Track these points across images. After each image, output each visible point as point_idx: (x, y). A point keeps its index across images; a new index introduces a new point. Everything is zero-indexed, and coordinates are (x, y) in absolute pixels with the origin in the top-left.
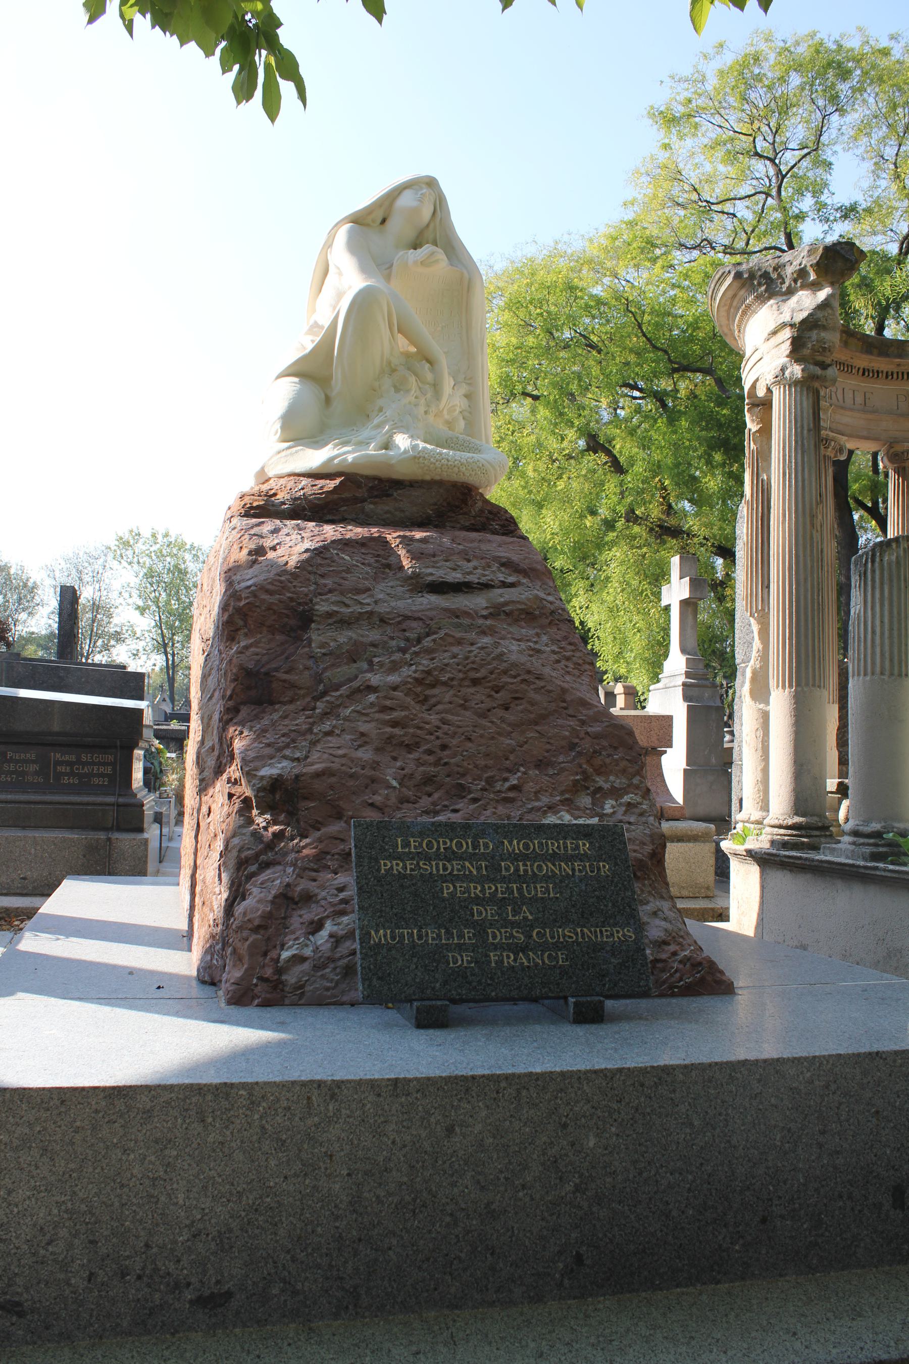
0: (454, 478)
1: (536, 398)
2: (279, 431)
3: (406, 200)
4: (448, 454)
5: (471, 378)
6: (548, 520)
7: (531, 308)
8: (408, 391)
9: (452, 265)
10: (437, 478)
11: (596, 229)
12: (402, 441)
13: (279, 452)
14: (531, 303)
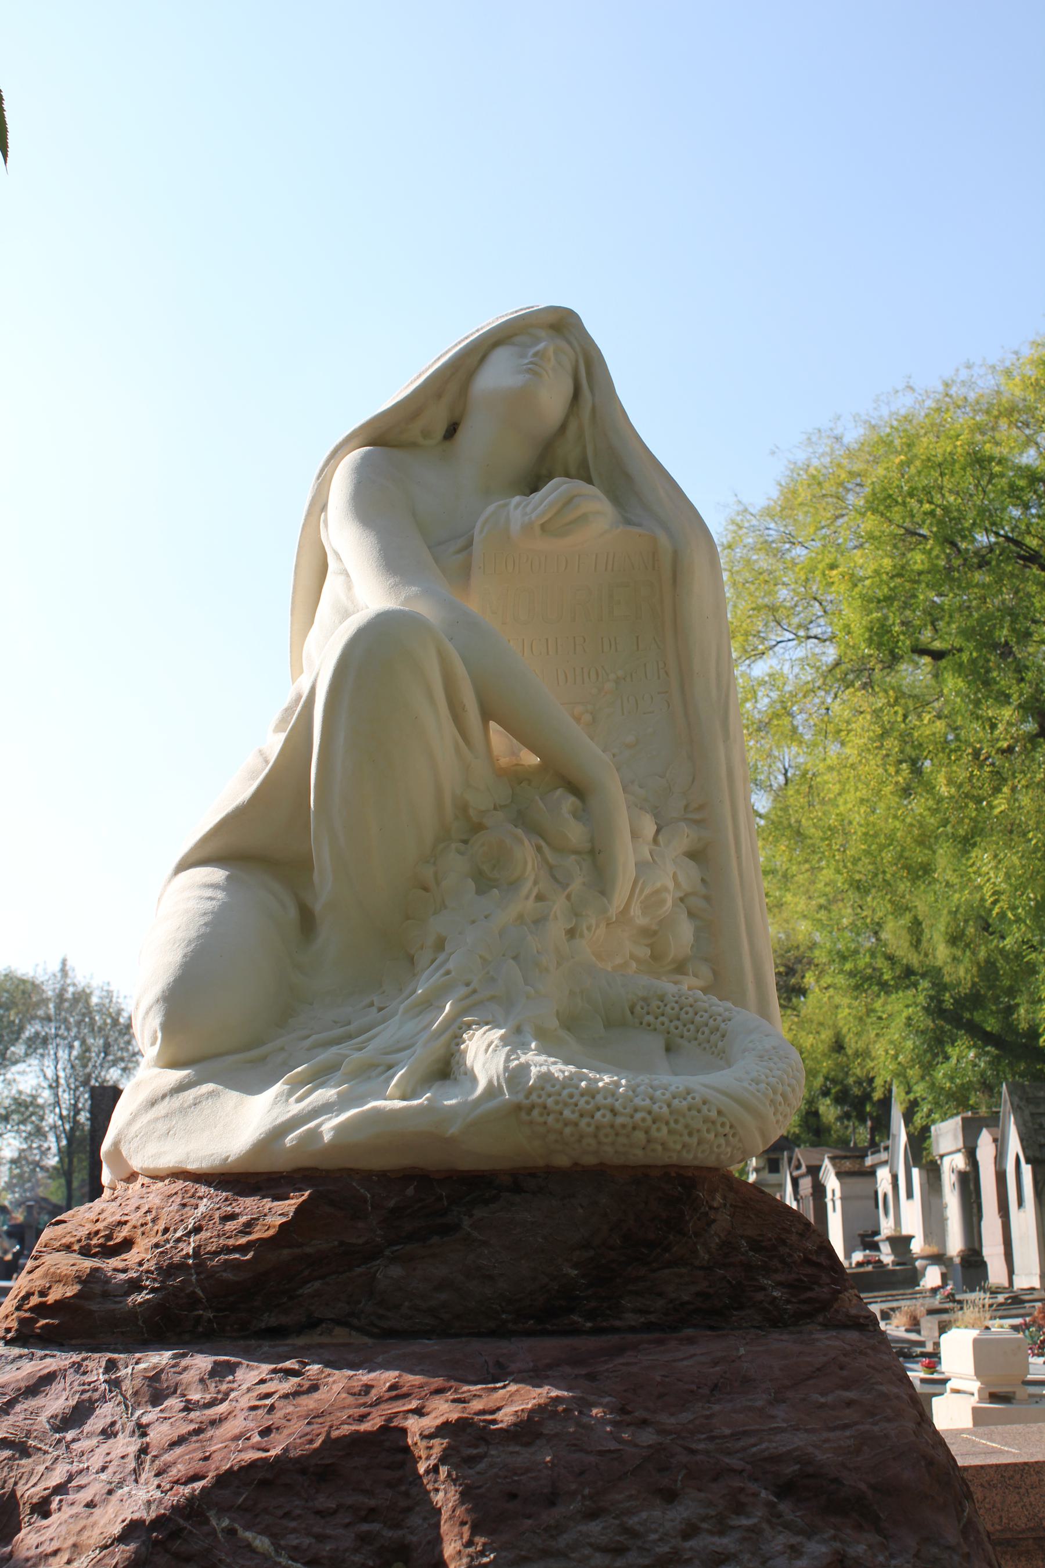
0: (638, 1156)
1: (937, 656)
2: (159, 1035)
3: (498, 375)
4: (611, 1092)
5: (701, 808)
6: (984, 869)
7: (913, 502)
8: (514, 885)
9: (628, 522)
10: (589, 1160)
11: (1016, 353)
12: (484, 1055)
13: (153, 1103)
14: (911, 495)
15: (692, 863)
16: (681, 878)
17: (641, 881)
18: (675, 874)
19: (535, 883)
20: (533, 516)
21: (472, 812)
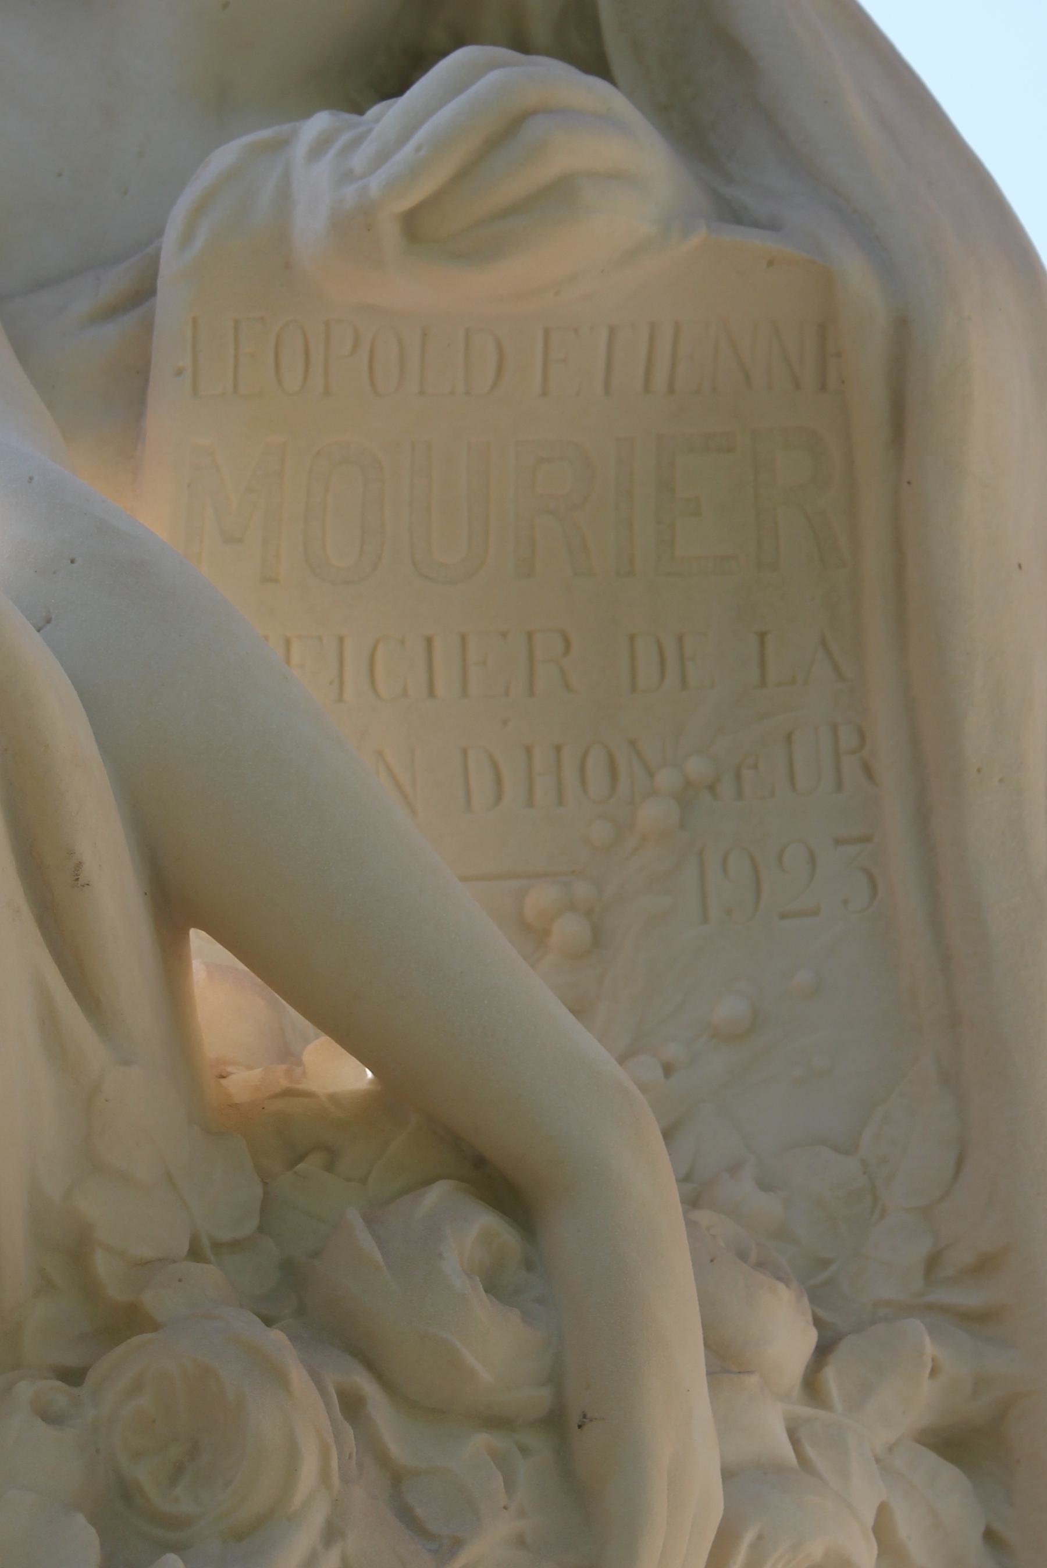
5: (984, 1266)
9: (733, 214)
15: (950, 1473)
16: (908, 1529)
17: (749, 1537)
18: (883, 1511)
19: (331, 1534)
20: (375, 183)
21: (103, 1265)
